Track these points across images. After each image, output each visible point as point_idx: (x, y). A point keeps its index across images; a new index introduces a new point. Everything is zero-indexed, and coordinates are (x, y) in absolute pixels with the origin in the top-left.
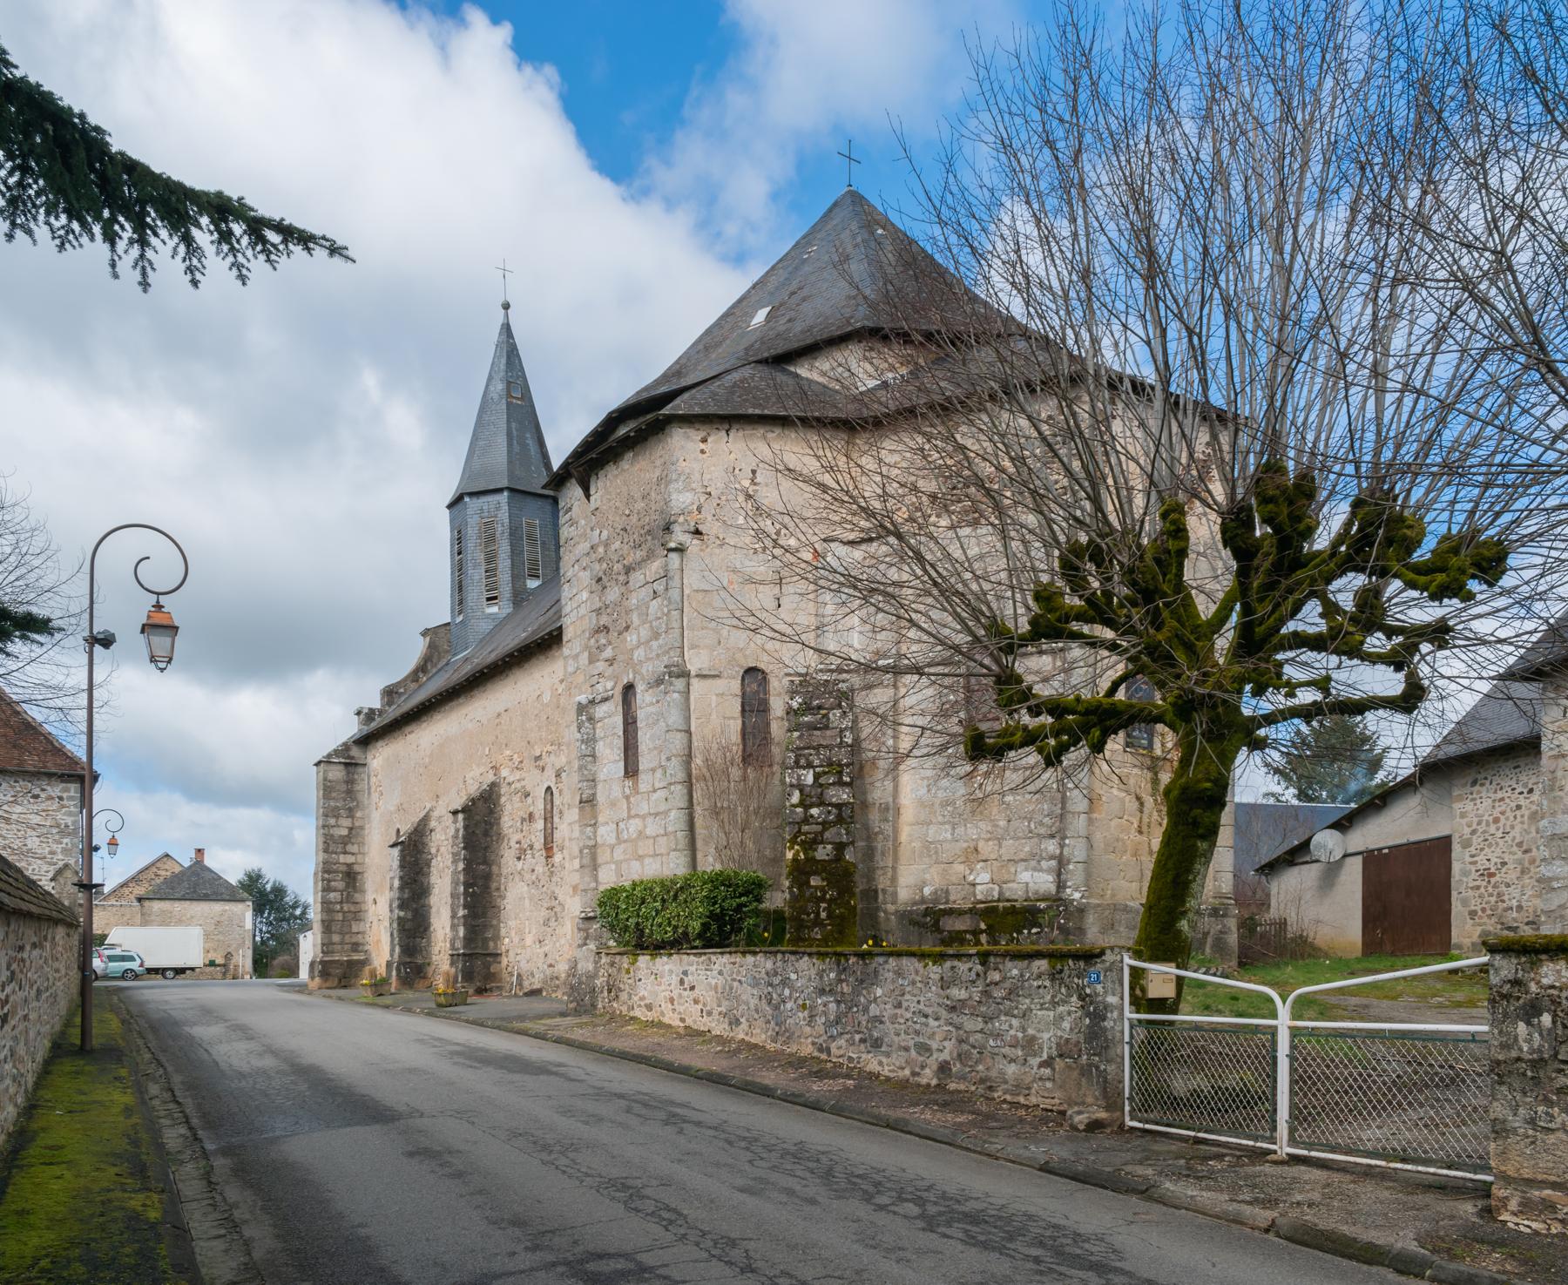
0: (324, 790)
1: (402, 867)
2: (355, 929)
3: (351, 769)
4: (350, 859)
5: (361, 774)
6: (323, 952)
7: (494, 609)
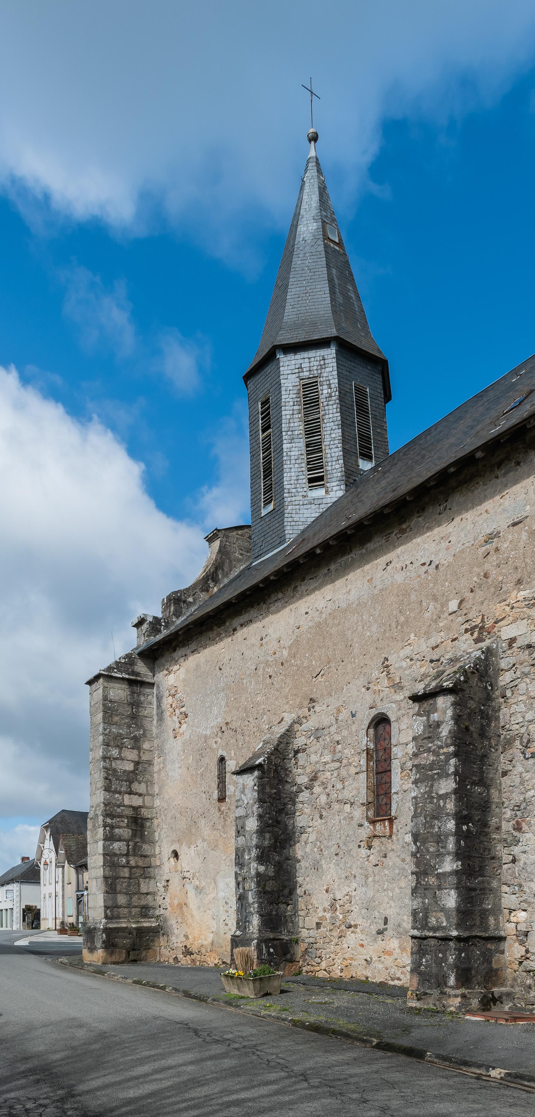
0: (105, 712)
1: (261, 801)
2: (144, 889)
3: (137, 689)
4: (137, 801)
5: (150, 697)
6: (106, 917)
7: (320, 492)
